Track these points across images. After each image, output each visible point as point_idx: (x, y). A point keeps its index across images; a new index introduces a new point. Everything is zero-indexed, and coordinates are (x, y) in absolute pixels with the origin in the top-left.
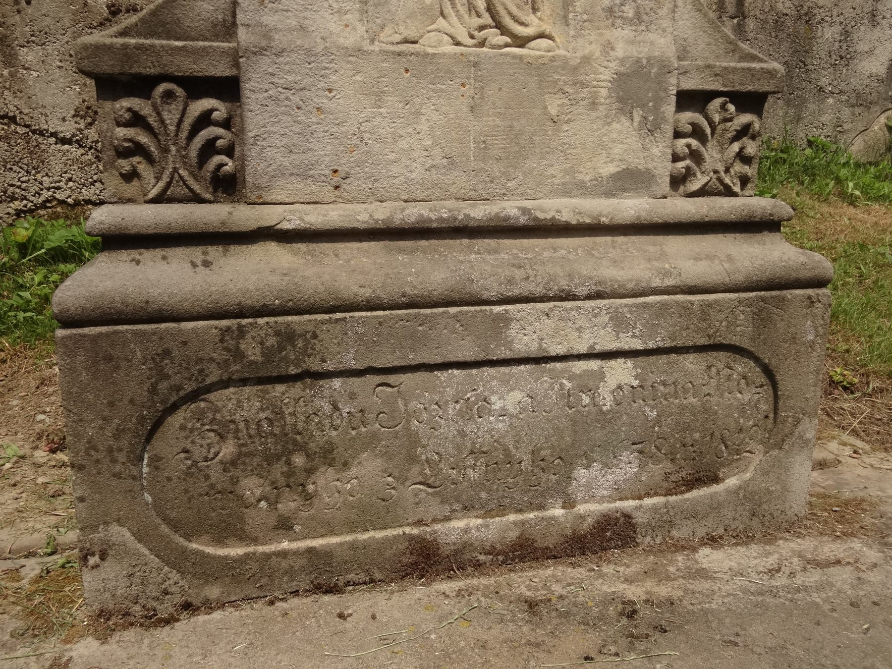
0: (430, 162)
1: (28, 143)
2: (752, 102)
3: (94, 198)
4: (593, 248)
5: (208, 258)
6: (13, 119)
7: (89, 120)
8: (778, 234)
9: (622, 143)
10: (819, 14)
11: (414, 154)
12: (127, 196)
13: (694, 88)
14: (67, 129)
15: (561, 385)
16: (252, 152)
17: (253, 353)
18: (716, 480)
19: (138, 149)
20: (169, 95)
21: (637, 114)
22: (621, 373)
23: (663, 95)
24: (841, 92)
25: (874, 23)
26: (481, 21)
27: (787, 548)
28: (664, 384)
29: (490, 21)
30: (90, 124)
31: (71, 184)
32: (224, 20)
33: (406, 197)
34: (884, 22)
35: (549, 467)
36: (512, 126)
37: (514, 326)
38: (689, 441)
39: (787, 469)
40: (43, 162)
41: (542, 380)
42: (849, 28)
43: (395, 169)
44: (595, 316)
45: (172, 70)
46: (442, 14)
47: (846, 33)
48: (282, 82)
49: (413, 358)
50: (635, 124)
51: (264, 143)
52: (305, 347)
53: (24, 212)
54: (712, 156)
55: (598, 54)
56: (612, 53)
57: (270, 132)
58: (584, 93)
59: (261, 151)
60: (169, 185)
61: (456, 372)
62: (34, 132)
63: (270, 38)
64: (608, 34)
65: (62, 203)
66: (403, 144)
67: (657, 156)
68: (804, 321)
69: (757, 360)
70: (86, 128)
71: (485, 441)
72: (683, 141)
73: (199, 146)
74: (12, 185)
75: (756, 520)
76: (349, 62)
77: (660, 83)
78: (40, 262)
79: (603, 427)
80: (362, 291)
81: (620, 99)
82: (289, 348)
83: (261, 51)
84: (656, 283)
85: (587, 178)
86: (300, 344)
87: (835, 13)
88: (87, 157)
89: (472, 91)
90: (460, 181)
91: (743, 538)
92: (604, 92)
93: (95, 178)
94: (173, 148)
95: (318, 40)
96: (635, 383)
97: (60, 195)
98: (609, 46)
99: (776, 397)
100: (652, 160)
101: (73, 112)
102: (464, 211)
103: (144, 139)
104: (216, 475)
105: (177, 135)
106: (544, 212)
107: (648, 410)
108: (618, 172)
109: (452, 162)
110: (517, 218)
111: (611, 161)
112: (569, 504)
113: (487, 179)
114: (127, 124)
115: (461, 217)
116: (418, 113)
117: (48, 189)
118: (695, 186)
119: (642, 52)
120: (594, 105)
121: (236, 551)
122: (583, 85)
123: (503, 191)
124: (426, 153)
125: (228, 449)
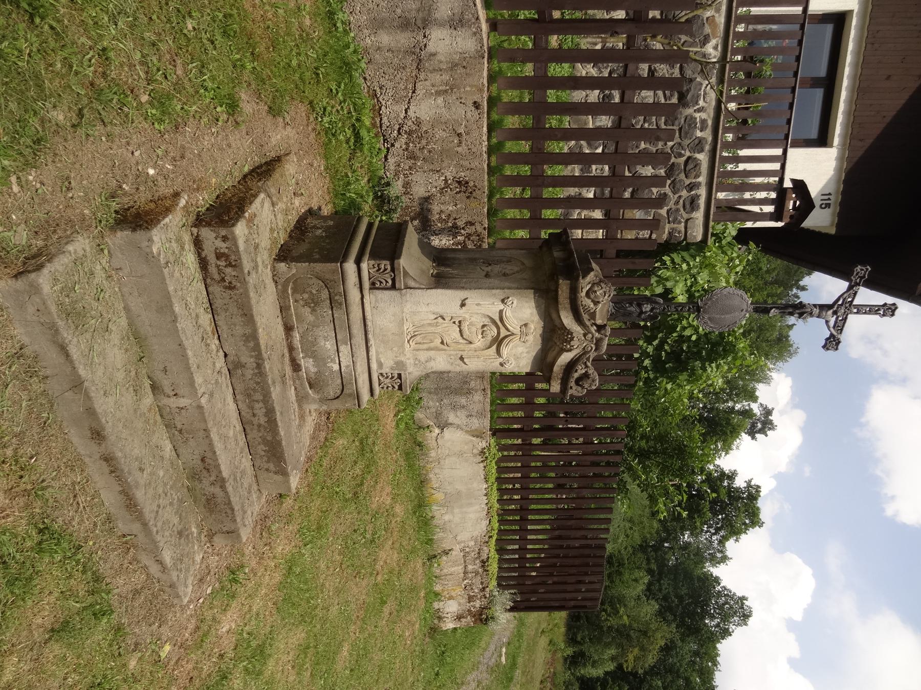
2: (400, 388)
6: (414, 92)
10: (470, 397)
14: (411, 113)
17: (337, 298)
19: (379, 269)
22: (336, 367)
25: (467, 416)
27: (296, 405)
35: (312, 351)
54: (388, 380)
68: (350, 404)
71: (318, 340)
90: (378, 331)
91: (297, 396)
104: (308, 289)
112: (303, 358)
119: (408, 366)
121: (290, 292)
125: (314, 292)
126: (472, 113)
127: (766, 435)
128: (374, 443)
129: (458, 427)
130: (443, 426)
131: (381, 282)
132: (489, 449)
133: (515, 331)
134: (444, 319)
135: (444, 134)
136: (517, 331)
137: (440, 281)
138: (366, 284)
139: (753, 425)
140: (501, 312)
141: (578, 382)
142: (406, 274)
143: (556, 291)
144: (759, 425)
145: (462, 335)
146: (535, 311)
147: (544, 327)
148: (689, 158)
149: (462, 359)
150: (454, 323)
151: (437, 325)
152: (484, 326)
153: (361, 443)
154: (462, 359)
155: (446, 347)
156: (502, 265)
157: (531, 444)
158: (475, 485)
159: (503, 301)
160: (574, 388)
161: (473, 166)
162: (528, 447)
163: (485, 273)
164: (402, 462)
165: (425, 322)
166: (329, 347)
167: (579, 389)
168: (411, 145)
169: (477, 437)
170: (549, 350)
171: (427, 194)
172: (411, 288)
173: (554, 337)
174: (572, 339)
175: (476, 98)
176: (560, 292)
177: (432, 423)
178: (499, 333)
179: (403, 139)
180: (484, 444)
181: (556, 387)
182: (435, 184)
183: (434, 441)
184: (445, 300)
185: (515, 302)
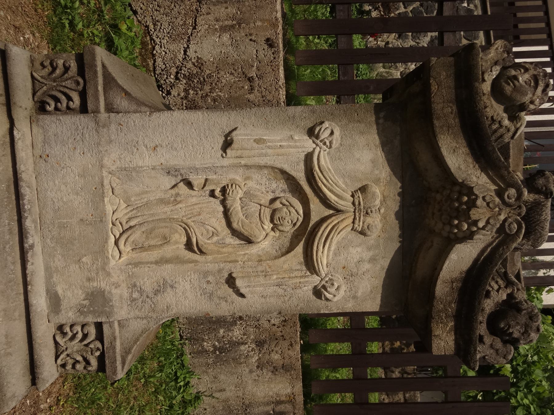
0: (56, 201)
1: (183, 34)
3: (157, 64)
4: (15, 283)
6: (194, 28)
7: (196, 64)
8: (30, 384)
9: (73, 296)
11: (59, 193)
12: (35, 63)
13: (104, 332)
14: (190, 53)
16: (54, 118)
19: (54, 69)
20: (78, 83)
21: (86, 302)
23: (97, 315)
26: (124, 224)
29: (125, 228)
30: (194, 64)
31: (164, 53)
32: (114, 108)
33: (38, 189)
36: (75, 240)
40: (174, 40)
43: (51, 183)
45: (88, 85)
48: (85, 132)
50: (82, 302)
51: (58, 124)
53: (148, 30)
55: (112, 280)
56: (113, 287)
57: (63, 126)
59: (54, 122)
60: (39, 81)
62: (189, 37)
63: (104, 127)
64: (124, 285)
65: (154, 48)
66: (63, 187)
67: (68, 315)
70: (192, 62)
72: (80, 330)
73: (57, 95)
74: (161, 25)
76: (96, 162)
78: (107, 34)
81: (92, 293)
83: (97, 123)
85: (54, 279)
88: (178, 62)
89: (90, 219)
92: (95, 284)
93: (167, 65)
94: (55, 84)
95: (105, 148)
97: (157, 47)
98: (117, 286)
100: (66, 313)
101: (199, 56)
102: (29, 216)
105: (61, 86)
106: (32, 256)
108: (58, 295)
110: (27, 243)
111: (64, 291)
113: (50, 229)
114: (64, 65)
115: (26, 215)
116: (77, 194)
117: (160, 42)
118: (58, 338)
119: (115, 301)
120: (89, 280)
122: (97, 273)
123: (45, 237)
124: (60, 198)
126: (265, 53)
133: (341, 204)
135: (232, 79)
136: (346, 204)
138: (24, 100)
140: (309, 157)
145: (229, 224)
146: (380, 155)
149: (231, 281)
150: (212, 194)
155: (197, 257)
159: (311, 133)
160: (488, 340)
165: (152, 197)
168: (191, 92)
173: (427, 209)
174: (472, 204)
175: (269, 34)
176: (434, 88)
179: (181, 86)
185: (337, 133)
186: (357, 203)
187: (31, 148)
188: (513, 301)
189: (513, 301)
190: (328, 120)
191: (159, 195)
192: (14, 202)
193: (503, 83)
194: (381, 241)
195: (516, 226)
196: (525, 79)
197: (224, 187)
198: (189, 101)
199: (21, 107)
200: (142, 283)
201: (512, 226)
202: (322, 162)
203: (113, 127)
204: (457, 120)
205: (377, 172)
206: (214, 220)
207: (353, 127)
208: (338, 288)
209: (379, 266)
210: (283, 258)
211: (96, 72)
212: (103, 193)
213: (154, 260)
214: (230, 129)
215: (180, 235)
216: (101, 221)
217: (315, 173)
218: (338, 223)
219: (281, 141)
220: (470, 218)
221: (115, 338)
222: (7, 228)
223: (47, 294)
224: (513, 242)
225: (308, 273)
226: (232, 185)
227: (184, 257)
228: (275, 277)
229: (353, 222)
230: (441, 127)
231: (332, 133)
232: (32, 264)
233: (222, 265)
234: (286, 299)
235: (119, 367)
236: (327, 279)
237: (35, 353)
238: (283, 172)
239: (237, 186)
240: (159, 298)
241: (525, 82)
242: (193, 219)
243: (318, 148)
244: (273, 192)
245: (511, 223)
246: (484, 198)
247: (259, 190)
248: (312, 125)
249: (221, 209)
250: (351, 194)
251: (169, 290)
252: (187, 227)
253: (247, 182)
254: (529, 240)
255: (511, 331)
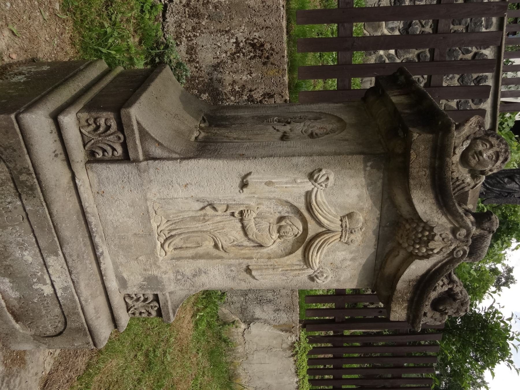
5: (59, 155)
11: (115, 217)
12: (81, 121)
15: (38, 272)
18: (17, 321)
19: (98, 127)
22: (48, 290)
24: (246, 302)
28: (47, 303)
29: (167, 237)
34: (276, 314)
37: (55, 258)
38: (29, 312)
39: (27, 343)
41: (37, 267)
42: (272, 302)
43: (109, 211)
44: (66, 282)
46: (168, 221)
47: (270, 301)
49: (35, 227)
52: (29, 194)
54: (139, 304)
55: (162, 270)
58: (148, 267)
61: (34, 240)
63: (144, 172)
66: (118, 213)
69: (64, 330)
75: (5, 335)
77: (157, 289)
79: (26, 286)
80: (55, 211)
81: (149, 278)
82: (28, 189)
83: (139, 170)
84: (82, 299)
86: (30, 192)
87: (278, 296)
90: (110, 231)
92: (150, 273)
94: (101, 139)
95: (147, 187)
96: (45, 295)
98: (165, 273)
99: (52, 336)
103: (101, 129)
107: (37, 299)
109: (115, 228)
115: (94, 235)
116: (130, 218)
122: (151, 266)
127: (509, 288)
128: (165, 353)
129: (265, 322)
130: (249, 321)
131: (104, 151)
132: (299, 344)
133: (332, 227)
134: (215, 209)
136: (335, 225)
137: (204, 148)
138: (79, 154)
139: (499, 280)
140: (308, 195)
141: (436, 305)
142: (144, 134)
143: (406, 155)
144: (503, 280)
145: (246, 234)
146: (365, 193)
147: (381, 219)
148: (476, 54)
149: (248, 270)
150: (233, 214)
151: (205, 220)
152: (281, 219)
153: (147, 355)
154: (248, 270)
155: (222, 253)
156: (308, 123)
157: (342, 336)
158: (286, 379)
159: (311, 176)
160: (429, 315)
161: (268, 23)
162: (340, 339)
163: (280, 134)
164: (205, 363)
165: (186, 215)
166: (30, 259)
167: (437, 315)
169: (286, 331)
170: (389, 254)
171: (216, 61)
172: (155, 159)
173: (398, 232)
174: (431, 238)
176: (413, 156)
177: (237, 319)
178: (305, 230)
180: (294, 338)
181: (399, 313)
182: (224, 48)
183: (240, 337)
184: (211, 179)
185: (332, 178)
186: (344, 226)
187: (89, 188)
188: (452, 293)
189: (452, 293)
190: (325, 168)
191: (191, 214)
192: (84, 226)
193: (470, 157)
194: (361, 248)
195: (462, 253)
196: (488, 154)
197: (242, 211)
198: (191, 8)
199: (78, 162)
200: (183, 270)
201: (459, 253)
202: (319, 198)
203: (151, 171)
204: (428, 180)
205: (361, 204)
206: (234, 232)
207: (345, 173)
208: (326, 278)
209: (358, 263)
210: (286, 258)
211: (133, 131)
212: (149, 217)
213: (190, 256)
214: (246, 173)
215: (210, 242)
216: (150, 235)
217: (313, 206)
218: (329, 238)
219: (286, 183)
220: (428, 246)
221: (167, 301)
222: (82, 243)
223: (116, 278)
224: (458, 263)
225: (305, 267)
226: (248, 211)
227: (213, 253)
228: (280, 269)
229: (341, 238)
230: (415, 185)
231: (328, 179)
232: (104, 264)
233: (241, 261)
234: (288, 281)
235: (171, 315)
236: (319, 271)
237: (114, 313)
238: (287, 202)
239: (252, 212)
240: (196, 279)
241: (489, 157)
242: (218, 231)
243: (316, 189)
244: (280, 213)
245: (459, 251)
246: (441, 235)
247: (269, 212)
248: (311, 171)
249: (240, 225)
250: (340, 218)
251: (203, 274)
252: (214, 238)
253: (259, 206)
254: (470, 258)
255: (446, 311)
